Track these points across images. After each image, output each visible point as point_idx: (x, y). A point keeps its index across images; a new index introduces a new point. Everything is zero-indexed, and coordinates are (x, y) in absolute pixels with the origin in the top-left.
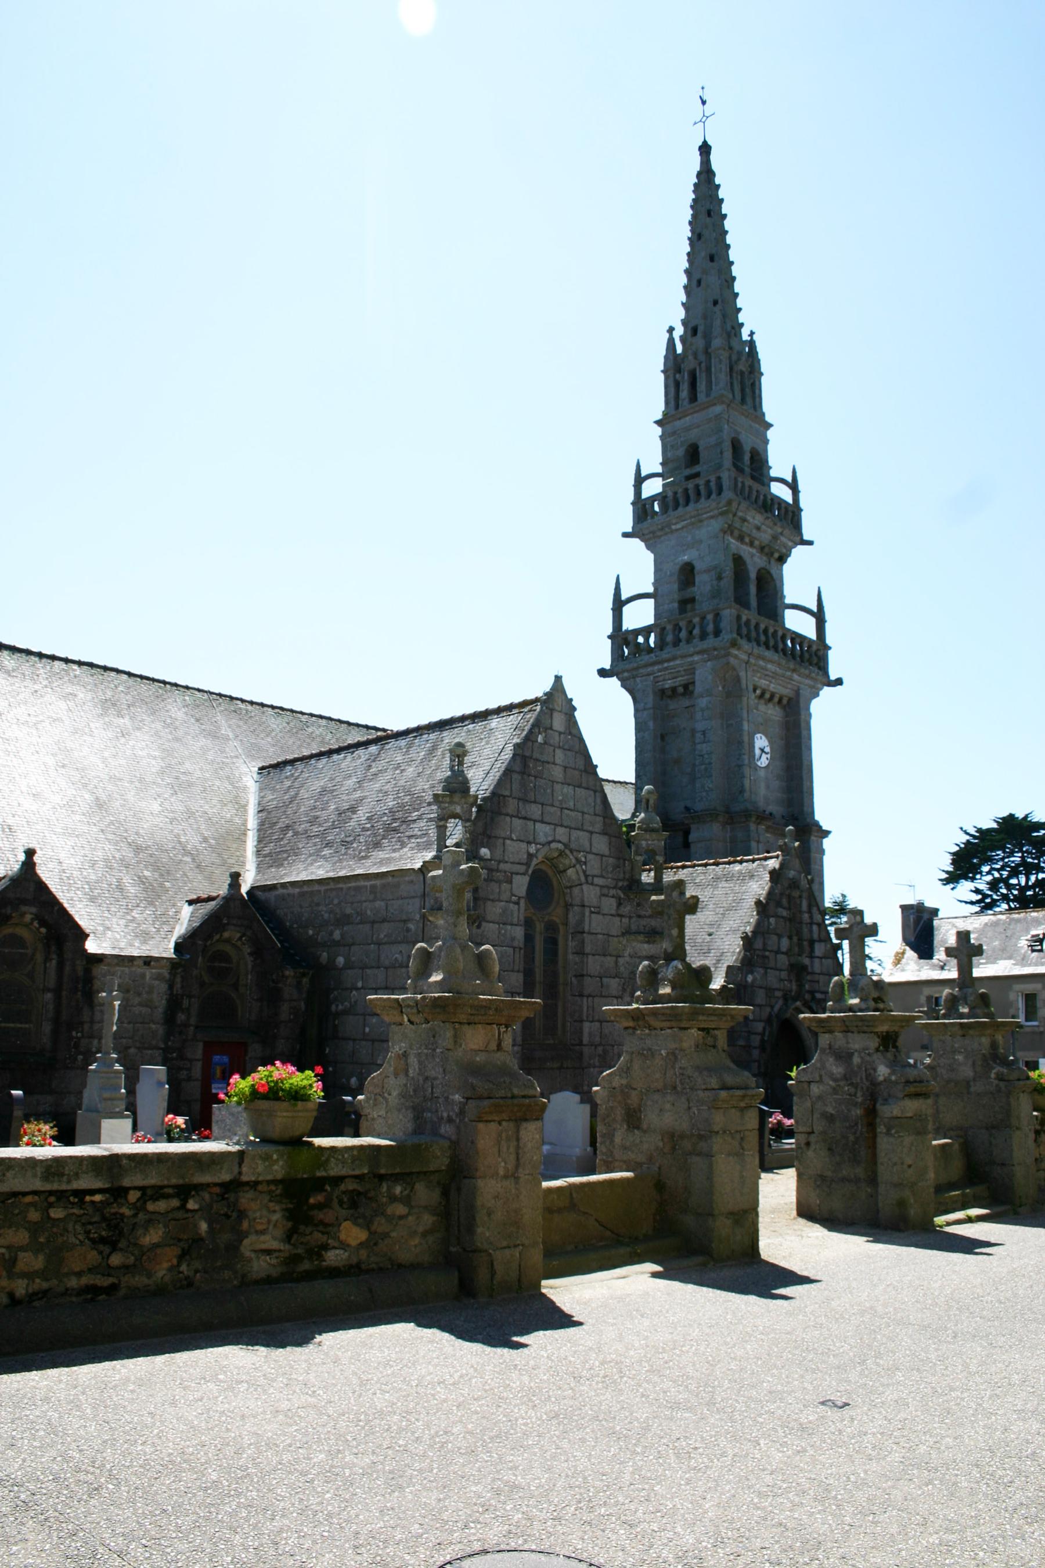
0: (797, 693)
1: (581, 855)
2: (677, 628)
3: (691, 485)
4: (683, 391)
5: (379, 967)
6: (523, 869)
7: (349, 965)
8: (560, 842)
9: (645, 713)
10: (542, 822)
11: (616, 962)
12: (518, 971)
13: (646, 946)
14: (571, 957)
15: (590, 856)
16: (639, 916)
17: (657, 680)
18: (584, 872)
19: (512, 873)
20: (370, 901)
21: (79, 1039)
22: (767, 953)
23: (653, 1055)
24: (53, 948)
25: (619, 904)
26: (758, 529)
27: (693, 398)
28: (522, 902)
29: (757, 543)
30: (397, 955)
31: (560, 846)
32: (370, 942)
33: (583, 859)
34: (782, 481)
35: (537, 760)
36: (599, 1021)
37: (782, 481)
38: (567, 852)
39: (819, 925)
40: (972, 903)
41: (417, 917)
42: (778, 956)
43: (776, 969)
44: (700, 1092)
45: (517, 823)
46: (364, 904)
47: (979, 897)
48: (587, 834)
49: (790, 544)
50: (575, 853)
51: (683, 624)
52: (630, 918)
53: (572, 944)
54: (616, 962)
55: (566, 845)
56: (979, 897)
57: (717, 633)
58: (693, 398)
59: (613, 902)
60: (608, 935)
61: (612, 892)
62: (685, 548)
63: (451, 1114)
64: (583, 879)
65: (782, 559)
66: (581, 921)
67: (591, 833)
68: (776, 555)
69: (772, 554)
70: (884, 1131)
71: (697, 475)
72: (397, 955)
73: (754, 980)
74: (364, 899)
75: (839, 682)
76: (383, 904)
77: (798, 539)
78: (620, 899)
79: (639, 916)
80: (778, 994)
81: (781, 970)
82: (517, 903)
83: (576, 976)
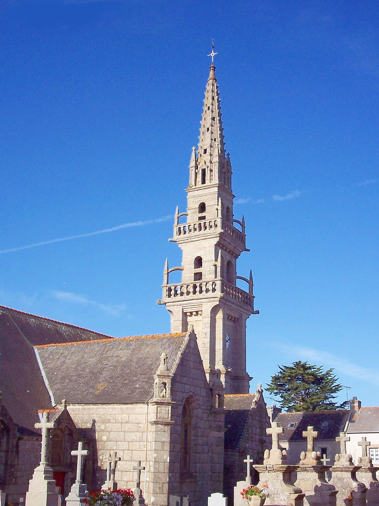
0: (241, 316)
1: (197, 397)
2: (195, 287)
3: (202, 222)
4: (199, 178)
5: (125, 441)
6: (181, 403)
7: (109, 440)
8: (192, 392)
9: (178, 322)
10: (187, 384)
11: (207, 439)
12: (179, 444)
13: (217, 433)
14: (192, 437)
15: (200, 397)
16: (215, 421)
17: (183, 308)
18: (198, 403)
19: (178, 405)
20: (120, 414)
21: (13, 472)
22: (253, 435)
23: (308, 480)
24: (5, 434)
25: (208, 416)
26: (229, 244)
27: (204, 182)
28: (181, 416)
29: (228, 250)
30: (134, 437)
31: (192, 393)
32: (120, 431)
33: (198, 399)
34: (238, 222)
35: (186, 360)
36: (201, 463)
37: (238, 222)
38: (194, 396)
39: (268, 423)
40: (279, 402)
41: (144, 422)
42: (256, 436)
43: (255, 441)
44: (325, 491)
45: (180, 384)
46: (117, 416)
47: (283, 399)
48: (199, 388)
49: (241, 250)
50: (196, 396)
51: (198, 285)
52: (211, 421)
53: (193, 432)
54: (207, 439)
55: (193, 393)
56: (283, 399)
57: (214, 290)
58: (204, 182)
59: (206, 415)
60: (205, 429)
61: (206, 411)
62: (198, 249)
63: (285, 498)
64: (198, 407)
65: (236, 257)
66: (196, 424)
67: (201, 388)
68: (235, 255)
69: (233, 254)
70: (355, 503)
71: (204, 218)
72: (134, 437)
73: (249, 446)
74: (117, 413)
75: (258, 312)
76: (127, 416)
77: (243, 249)
78: (208, 414)
79: (215, 421)
80: (256, 451)
81: (257, 442)
82: (179, 417)
83: (194, 445)
